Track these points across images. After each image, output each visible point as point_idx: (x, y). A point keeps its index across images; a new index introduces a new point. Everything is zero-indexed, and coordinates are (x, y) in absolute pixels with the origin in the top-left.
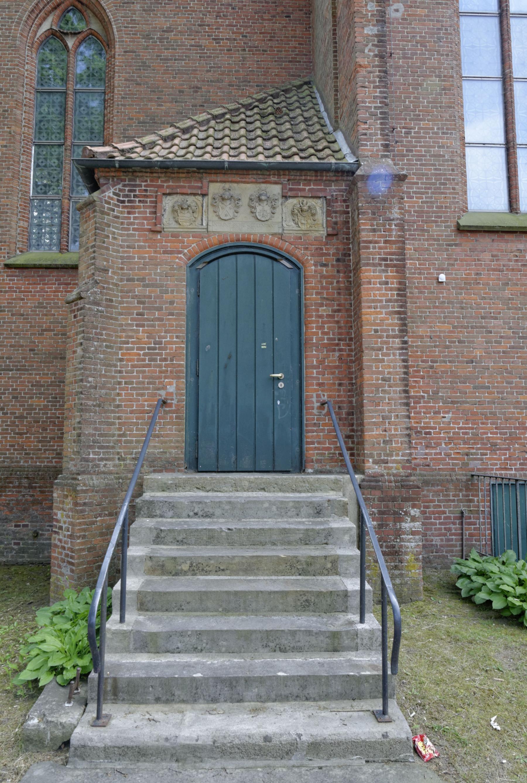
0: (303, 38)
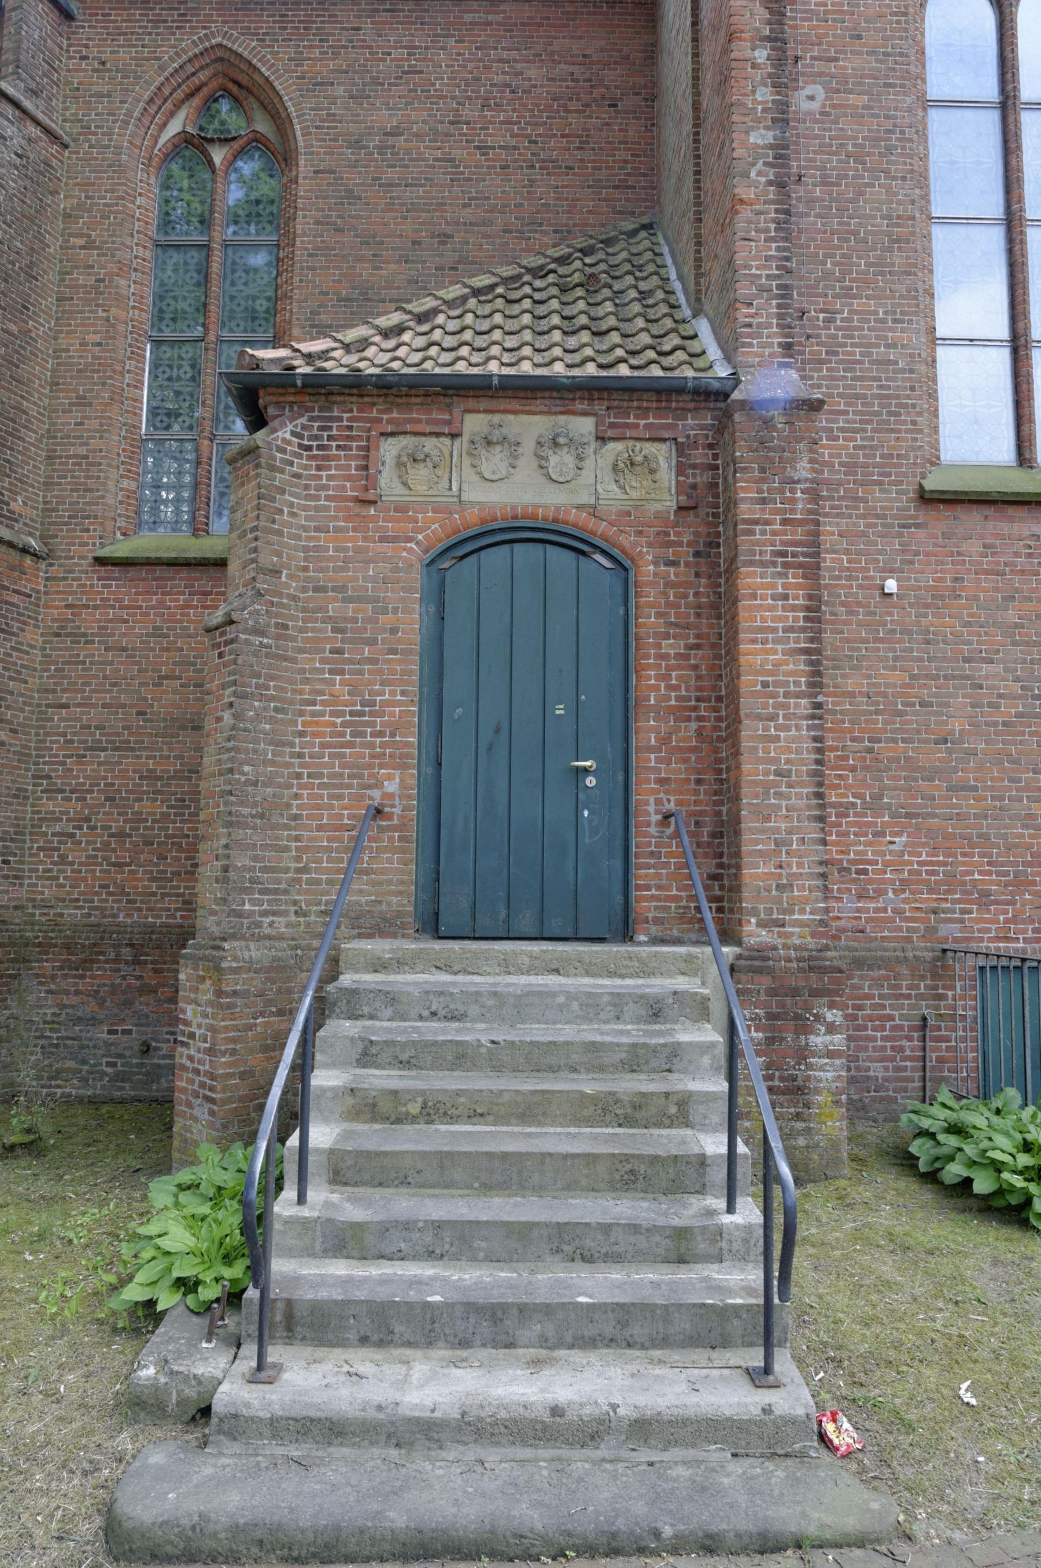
0: (639, 144)
